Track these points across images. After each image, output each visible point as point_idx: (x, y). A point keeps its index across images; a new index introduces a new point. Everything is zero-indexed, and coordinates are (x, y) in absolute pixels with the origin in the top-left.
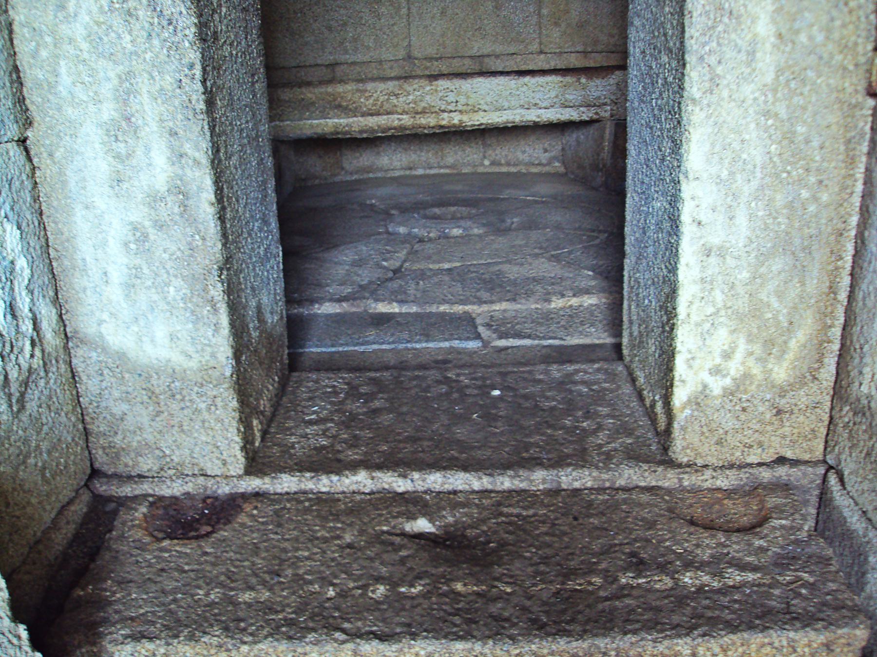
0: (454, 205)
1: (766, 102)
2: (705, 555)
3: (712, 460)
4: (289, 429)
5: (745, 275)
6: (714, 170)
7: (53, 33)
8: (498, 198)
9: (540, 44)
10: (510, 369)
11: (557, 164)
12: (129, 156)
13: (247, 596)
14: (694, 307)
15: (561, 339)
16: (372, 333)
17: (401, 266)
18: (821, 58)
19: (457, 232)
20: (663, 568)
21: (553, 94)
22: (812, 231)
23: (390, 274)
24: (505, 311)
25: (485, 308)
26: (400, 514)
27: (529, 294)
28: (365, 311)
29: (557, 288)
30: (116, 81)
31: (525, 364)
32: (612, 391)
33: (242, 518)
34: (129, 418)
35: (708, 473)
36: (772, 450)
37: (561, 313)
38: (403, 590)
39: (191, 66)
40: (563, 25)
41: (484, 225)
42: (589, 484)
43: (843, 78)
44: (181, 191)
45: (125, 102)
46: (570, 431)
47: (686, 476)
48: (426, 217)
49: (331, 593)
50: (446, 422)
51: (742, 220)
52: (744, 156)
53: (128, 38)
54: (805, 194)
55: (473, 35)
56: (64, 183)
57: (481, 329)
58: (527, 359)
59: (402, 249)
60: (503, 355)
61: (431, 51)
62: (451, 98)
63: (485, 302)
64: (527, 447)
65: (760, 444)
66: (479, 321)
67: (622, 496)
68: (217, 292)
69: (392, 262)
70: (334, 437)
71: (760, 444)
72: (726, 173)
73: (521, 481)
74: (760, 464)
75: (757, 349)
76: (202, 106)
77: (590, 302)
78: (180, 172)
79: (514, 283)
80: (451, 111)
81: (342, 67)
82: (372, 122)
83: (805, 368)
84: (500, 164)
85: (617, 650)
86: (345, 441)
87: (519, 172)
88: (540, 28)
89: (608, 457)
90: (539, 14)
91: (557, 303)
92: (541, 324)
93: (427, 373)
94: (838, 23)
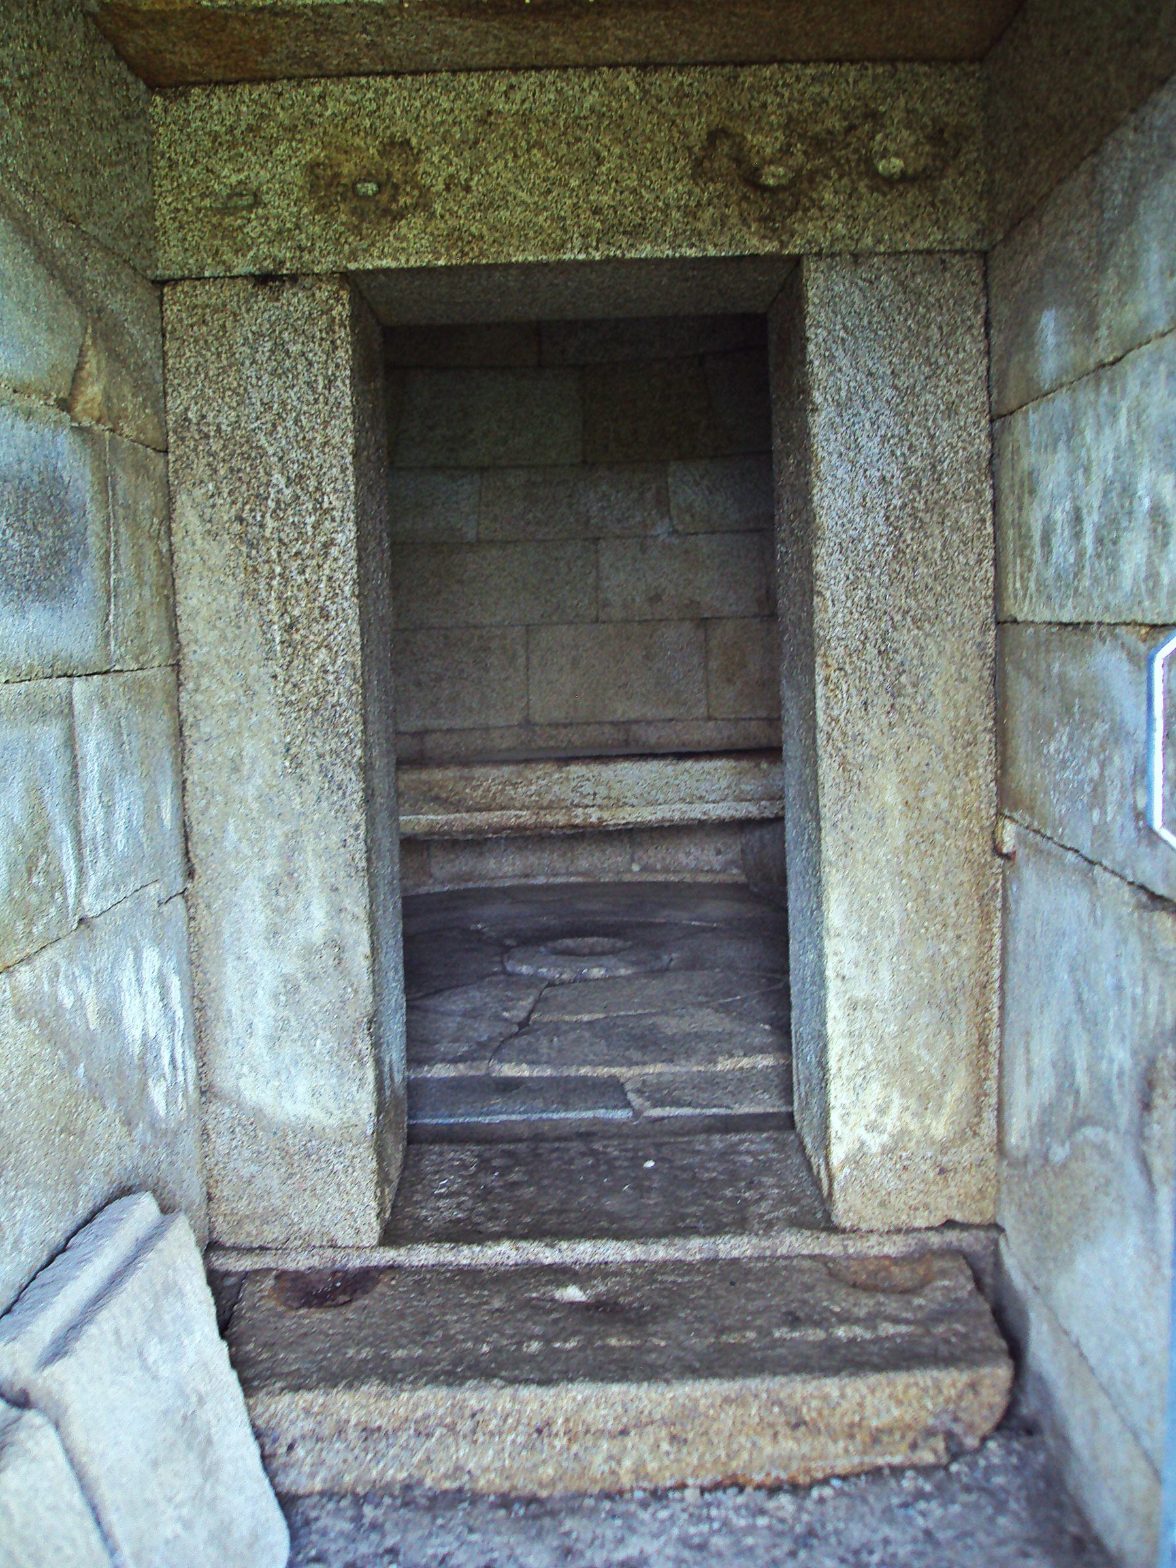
0: (592, 935)
1: (899, 864)
2: (862, 1313)
3: (876, 1224)
4: (417, 1202)
5: (893, 1028)
6: (854, 927)
7: (225, 793)
8: (651, 924)
9: (708, 706)
10: (666, 1139)
11: (735, 871)
12: (287, 910)
13: (401, 1353)
14: (845, 1061)
15: (728, 1107)
16: (497, 1101)
17: (528, 1018)
18: (947, 823)
19: (597, 973)
20: (817, 1324)
21: (724, 783)
22: (956, 983)
23: (515, 1029)
24: (660, 1074)
25: (636, 1071)
26: (548, 1283)
27: (689, 1054)
28: (488, 1075)
29: (725, 1046)
30: (282, 839)
31: (684, 1135)
32: (779, 1161)
33: (380, 1288)
34: (258, 1180)
35: (874, 1239)
36: (939, 1213)
37: (729, 1076)
38: (557, 1345)
39: (357, 827)
40: (739, 684)
41: (634, 963)
42: (748, 1253)
43: (970, 839)
44: (337, 946)
45: (289, 859)
46: (731, 1201)
47: (850, 1243)
48: (555, 952)
49: (485, 1348)
50: (594, 1195)
51: (885, 974)
52: (882, 913)
53: (298, 800)
54: (945, 949)
55: (616, 694)
56: (219, 934)
57: (631, 1096)
58: (689, 1128)
59: (528, 995)
60: (657, 1126)
61: (558, 715)
62: (588, 788)
63: (637, 1064)
64: (683, 1217)
65: (926, 1206)
66: (628, 1087)
67: (782, 1263)
68: (364, 1045)
69: (515, 1012)
70: (472, 1210)
71: (926, 1206)
72: (865, 929)
73: (677, 1250)
74: (928, 1229)
75: (913, 1103)
76: (364, 864)
77: (765, 1063)
78: (337, 926)
79: (672, 1040)
80: (587, 806)
81: (434, 736)
82: (479, 819)
83: (964, 1125)
84: (654, 871)
85: (768, 1391)
86: (482, 1213)
87: (681, 882)
88: (708, 686)
89: (770, 1225)
90: (705, 667)
91: (724, 1065)
92: (704, 1090)
93: (570, 1144)
94: (960, 791)
